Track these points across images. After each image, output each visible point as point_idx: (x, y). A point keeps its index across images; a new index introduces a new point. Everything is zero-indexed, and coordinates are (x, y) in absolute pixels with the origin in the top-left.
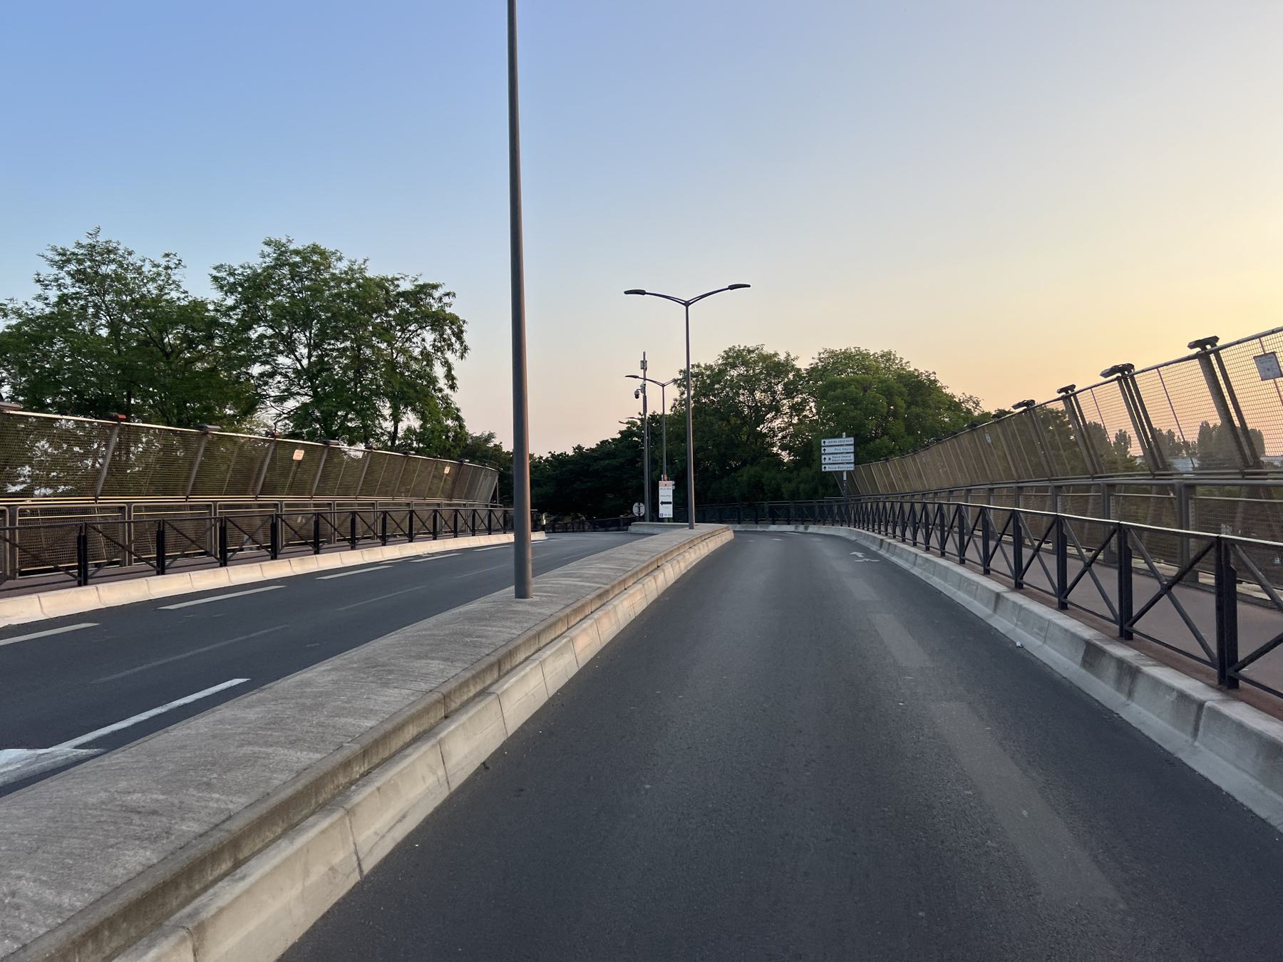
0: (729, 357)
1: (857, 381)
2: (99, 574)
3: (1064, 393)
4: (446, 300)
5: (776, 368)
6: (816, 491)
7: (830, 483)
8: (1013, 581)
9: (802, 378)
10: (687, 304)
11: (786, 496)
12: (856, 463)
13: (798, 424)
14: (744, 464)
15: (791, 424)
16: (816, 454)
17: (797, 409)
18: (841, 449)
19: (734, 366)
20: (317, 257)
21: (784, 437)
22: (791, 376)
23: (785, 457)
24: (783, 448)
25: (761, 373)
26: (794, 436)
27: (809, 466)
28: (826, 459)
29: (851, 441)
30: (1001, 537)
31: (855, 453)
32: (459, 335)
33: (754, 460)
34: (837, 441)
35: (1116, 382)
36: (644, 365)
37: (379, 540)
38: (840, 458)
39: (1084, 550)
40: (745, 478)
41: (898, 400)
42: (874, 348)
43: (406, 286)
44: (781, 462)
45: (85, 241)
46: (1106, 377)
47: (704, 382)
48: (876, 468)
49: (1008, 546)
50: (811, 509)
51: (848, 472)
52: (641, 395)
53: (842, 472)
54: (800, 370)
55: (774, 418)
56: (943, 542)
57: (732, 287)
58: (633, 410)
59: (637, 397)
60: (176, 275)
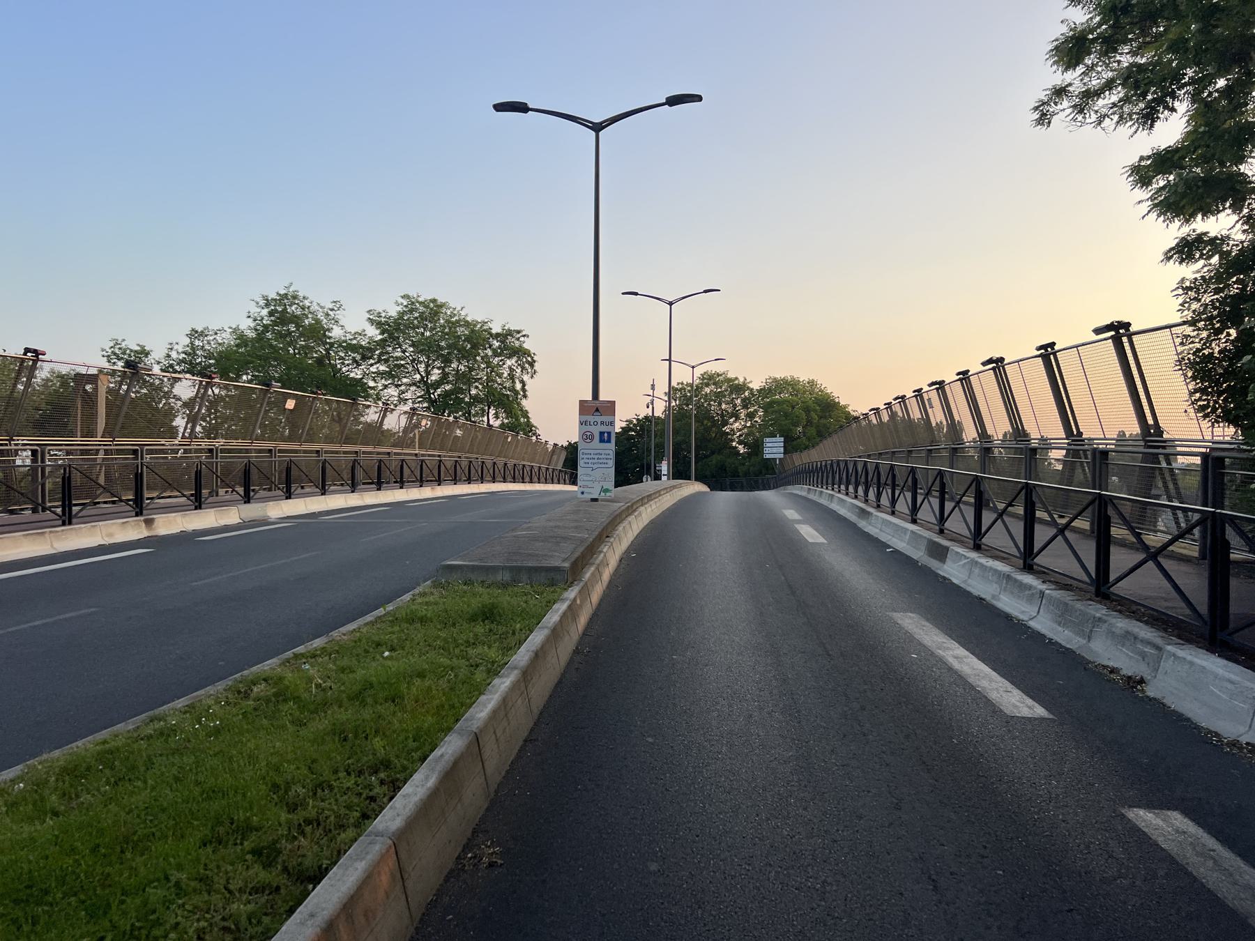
0: (703, 379)
1: (789, 402)
2: (84, 513)
3: (1043, 351)
4: (522, 339)
5: (738, 388)
6: (761, 473)
7: (768, 465)
8: (972, 542)
9: (754, 395)
10: (671, 304)
11: (741, 474)
12: (784, 453)
13: (749, 427)
14: (713, 453)
15: (745, 426)
16: (761, 447)
17: (751, 416)
18: (776, 445)
19: (707, 385)
20: (434, 310)
21: (741, 435)
22: (747, 394)
23: (741, 449)
24: (740, 443)
25: (726, 390)
26: (747, 435)
27: (757, 455)
28: (766, 450)
29: (782, 439)
30: (961, 498)
31: (784, 447)
32: (532, 364)
33: (720, 452)
34: (774, 439)
35: (1110, 341)
36: (653, 387)
37: (349, 488)
38: (775, 450)
39: (1055, 516)
40: (714, 462)
41: (813, 414)
42: (803, 377)
43: (496, 329)
44: (738, 453)
45: (282, 292)
46: (1097, 335)
47: (685, 396)
48: (796, 456)
49: (968, 507)
50: (756, 482)
51: (780, 459)
52: (651, 406)
53: (776, 459)
54: (752, 389)
55: (735, 422)
56: (894, 501)
57: (706, 291)
58: (644, 412)
59: (648, 407)
60: (339, 315)
